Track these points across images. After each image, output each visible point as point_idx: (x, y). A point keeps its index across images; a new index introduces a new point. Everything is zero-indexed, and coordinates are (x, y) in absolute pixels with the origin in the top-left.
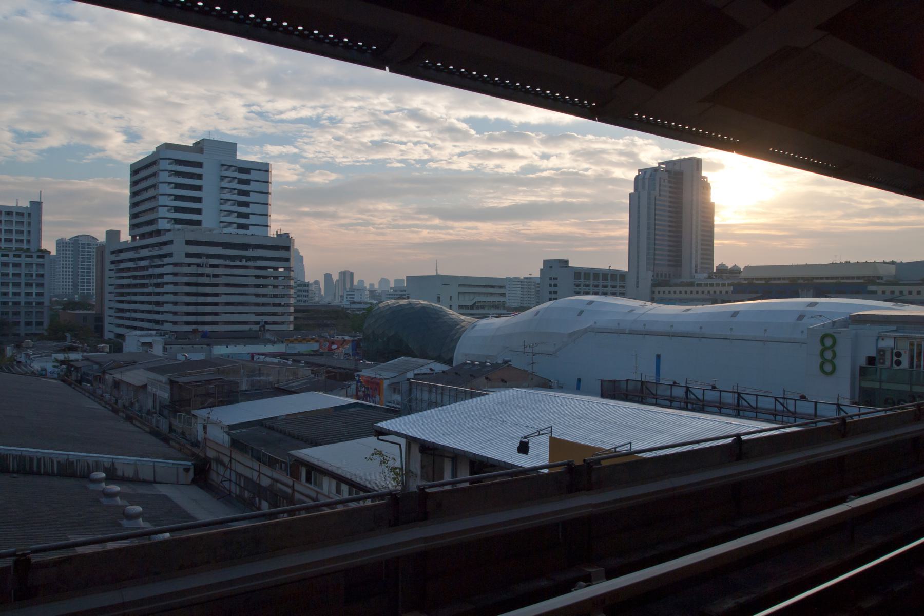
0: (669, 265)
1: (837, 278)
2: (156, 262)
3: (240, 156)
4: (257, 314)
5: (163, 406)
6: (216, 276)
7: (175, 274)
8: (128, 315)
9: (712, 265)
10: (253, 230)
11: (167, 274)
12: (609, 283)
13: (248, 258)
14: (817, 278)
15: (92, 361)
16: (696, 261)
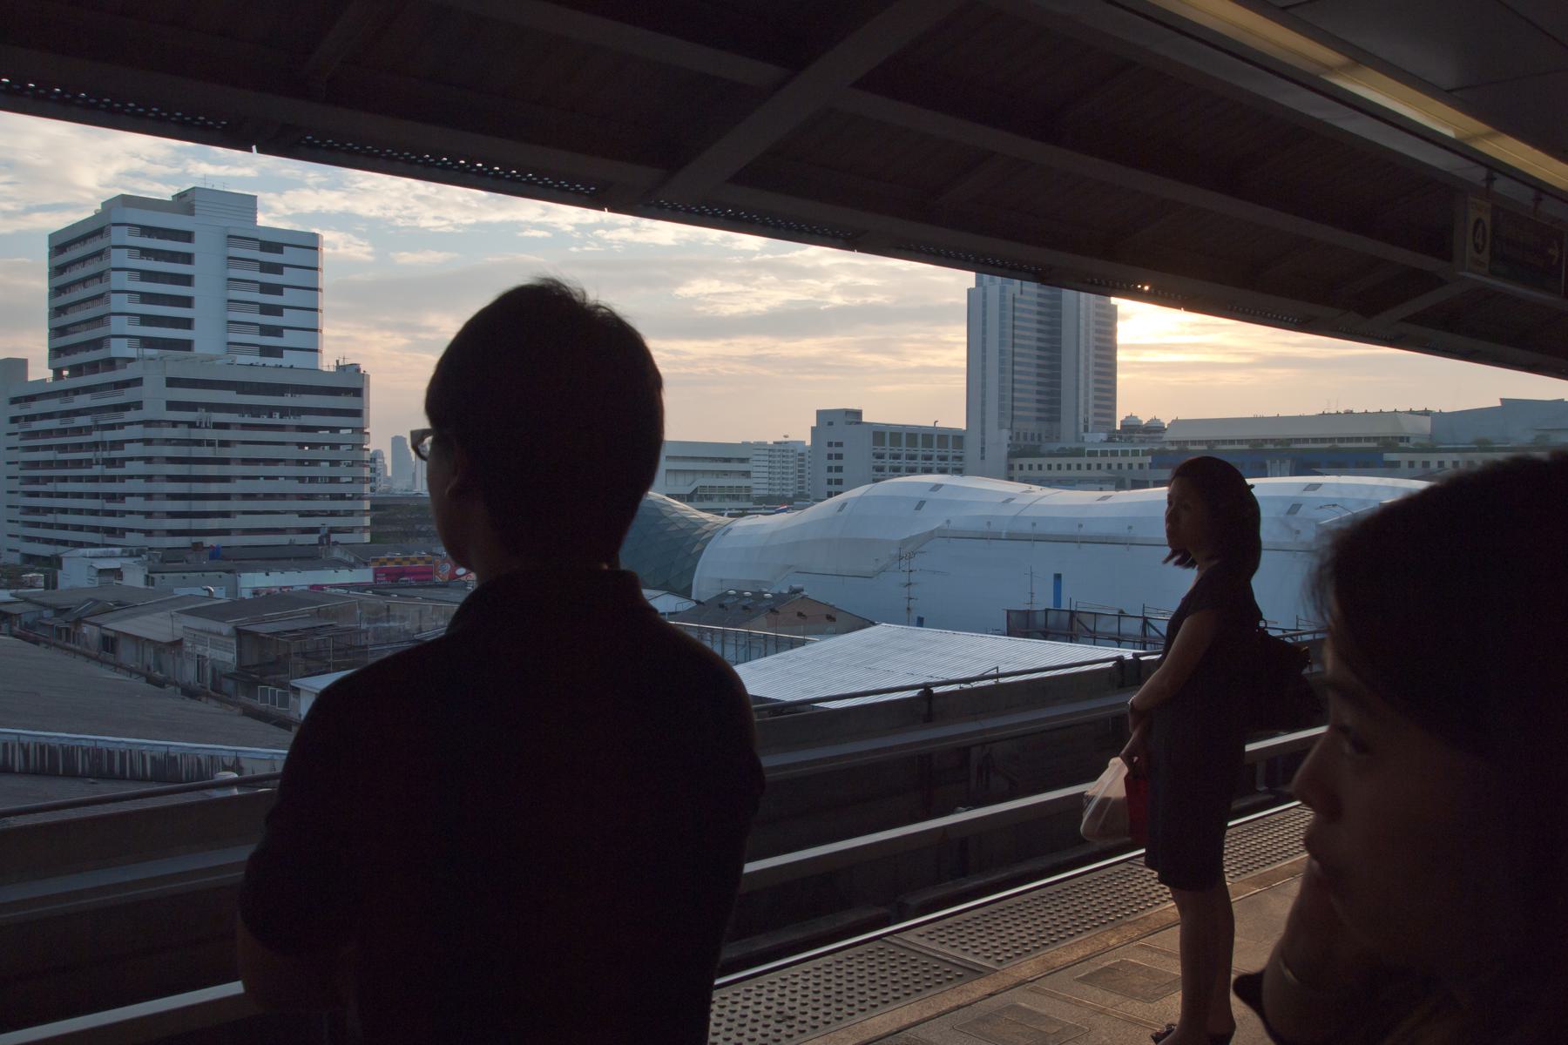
0: (1039, 419)
1: (1331, 440)
2: (106, 419)
3: (262, 220)
4: (302, 514)
5: (219, 677)
6: (224, 444)
7: (148, 442)
8: (50, 518)
9: (1113, 416)
10: (289, 359)
11: (131, 441)
12: (935, 451)
13: (284, 411)
14: (1298, 440)
15: (36, 603)
16: (1086, 411)
